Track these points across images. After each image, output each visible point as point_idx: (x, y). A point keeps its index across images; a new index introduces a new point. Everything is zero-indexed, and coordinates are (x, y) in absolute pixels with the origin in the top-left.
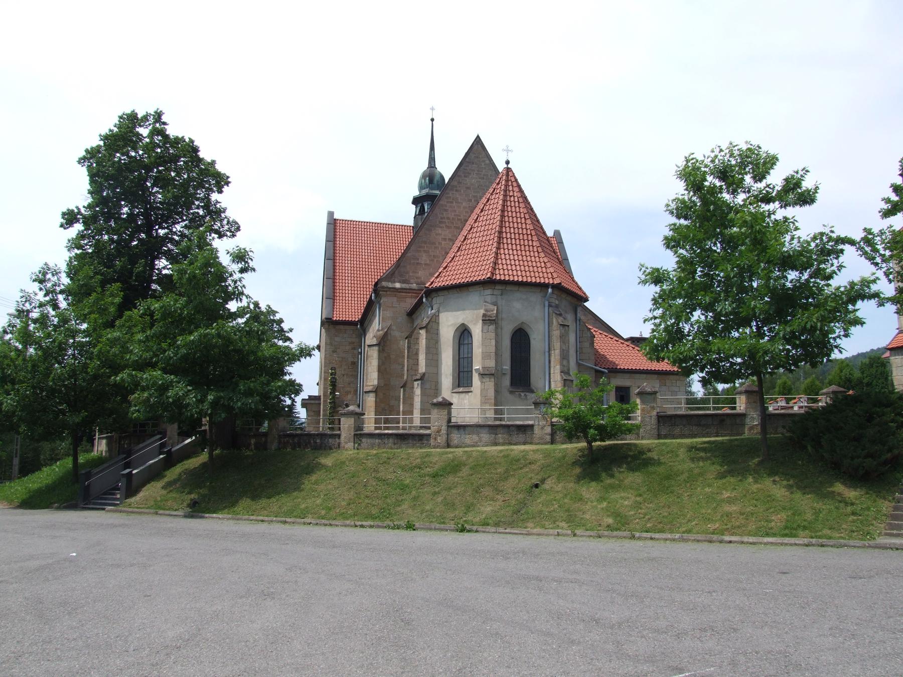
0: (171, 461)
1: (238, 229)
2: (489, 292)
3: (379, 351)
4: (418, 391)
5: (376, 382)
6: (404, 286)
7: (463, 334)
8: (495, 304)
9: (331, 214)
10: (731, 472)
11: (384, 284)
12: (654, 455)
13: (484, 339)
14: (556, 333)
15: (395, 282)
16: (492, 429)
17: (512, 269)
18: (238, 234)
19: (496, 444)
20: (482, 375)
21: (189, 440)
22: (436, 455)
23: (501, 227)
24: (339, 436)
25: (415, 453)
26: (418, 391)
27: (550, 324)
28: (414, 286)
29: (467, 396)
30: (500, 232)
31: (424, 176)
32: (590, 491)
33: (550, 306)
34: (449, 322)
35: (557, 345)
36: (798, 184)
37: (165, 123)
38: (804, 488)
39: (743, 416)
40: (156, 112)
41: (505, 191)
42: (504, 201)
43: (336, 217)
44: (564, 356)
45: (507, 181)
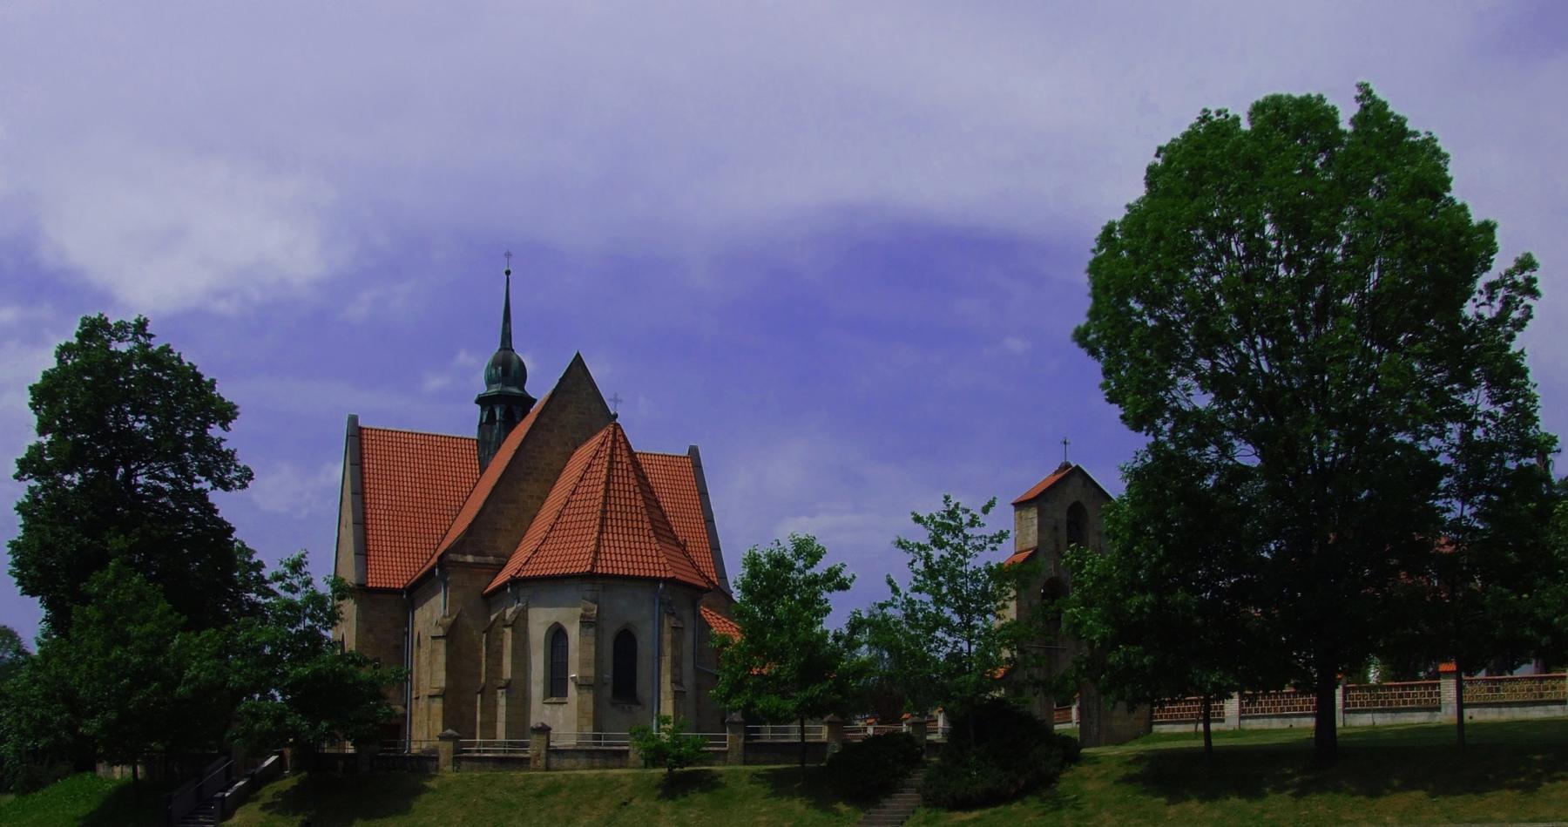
0: (258, 782)
1: (250, 477)
2: (588, 586)
3: (447, 646)
4: (502, 701)
5: (443, 684)
6: (478, 559)
7: (557, 635)
8: (595, 601)
9: (353, 420)
10: (774, 794)
11: (452, 556)
12: (723, 780)
13: (582, 644)
14: (667, 636)
15: (465, 554)
16: (590, 754)
17: (617, 561)
18: (250, 484)
19: (592, 767)
20: (579, 686)
21: (267, 763)
22: (539, 777)
23: (605, 504)
24: (437, 759)
25: (519, 775)
26: (502, 701)
27: (661, 625)
28: (491, 559)
29: (561, 708)
30: (604, 512)
31: (494, 364)
32: (666, 807)
33: (661, 603)
34: (540, 620)
35: (668, 650)
36: (837, 574)
37: (151, 336)
38: (816, 806)
39: (824, 745)
40: (138, 321)
41: (611, 456)
42: (610, 469)
43: (360, 424)
44: (676, 663)
45: (614, 441)
